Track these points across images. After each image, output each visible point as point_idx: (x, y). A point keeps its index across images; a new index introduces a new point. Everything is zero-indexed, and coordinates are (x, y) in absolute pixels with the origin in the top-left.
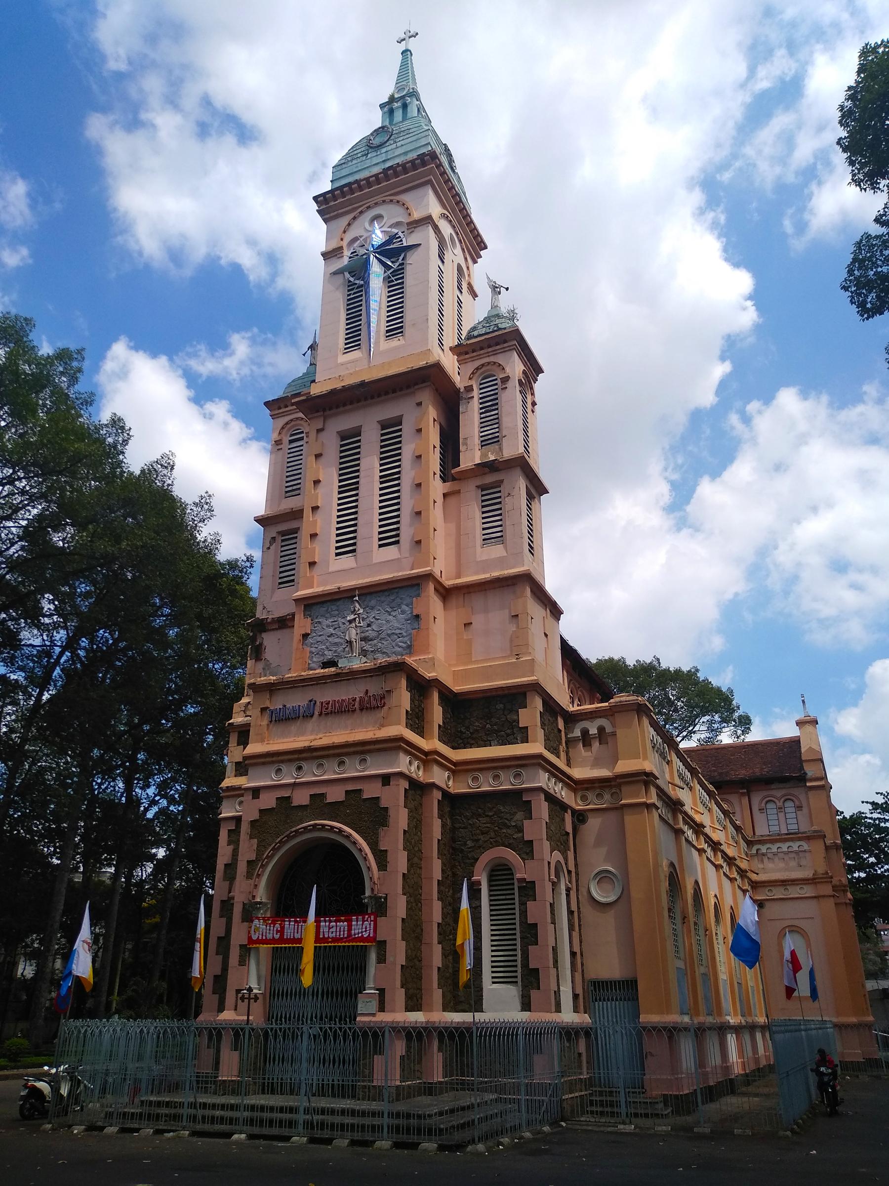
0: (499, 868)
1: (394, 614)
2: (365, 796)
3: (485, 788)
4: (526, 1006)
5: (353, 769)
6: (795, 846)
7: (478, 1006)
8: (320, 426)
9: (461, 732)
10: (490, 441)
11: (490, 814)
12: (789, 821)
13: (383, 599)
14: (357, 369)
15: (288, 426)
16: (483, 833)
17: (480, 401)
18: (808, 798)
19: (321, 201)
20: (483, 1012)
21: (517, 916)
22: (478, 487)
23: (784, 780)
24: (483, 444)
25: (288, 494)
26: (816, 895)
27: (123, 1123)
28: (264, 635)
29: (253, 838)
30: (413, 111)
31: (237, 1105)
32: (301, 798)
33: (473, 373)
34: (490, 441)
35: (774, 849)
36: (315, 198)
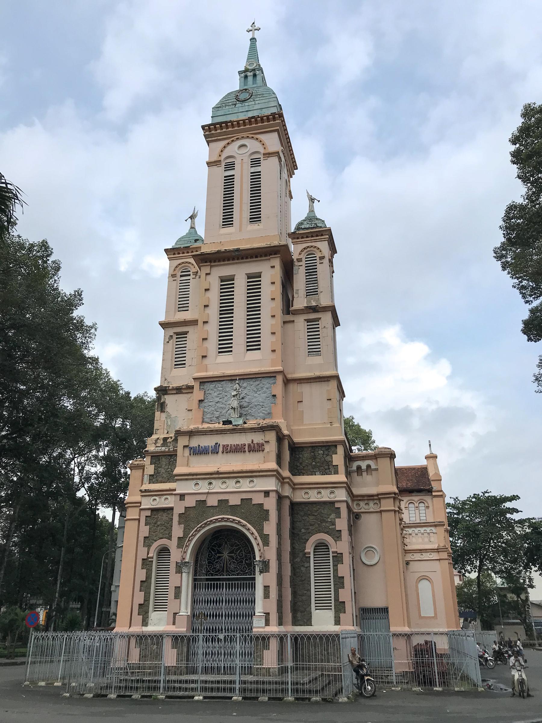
0: (320, 545)
1: (258, 393)
2: (253, 503)
3: (313, 499)
4: (337, 622)
5: (245, 485)
6: (428, 529)
7: (308, 623)
8: (208, 272)
9: (297, 466)
10: (312, 292)
11: (316, 514)
12: (421, 515)
13: (251, 383)
14: (231, 239)
15: (180, 266)
16: (311, 525)
17: (306, 268)
18: (433, 502)
19: (206, 129)
20: (311, 626)
21: (332, 572)
22: (305, 320)
23: (420, 491)
24: (308, 294)
25: (180, 309)
26: (438, 558)
27: (119, 692)
28: (166, 396)
29: (181, 524)
30: (259, 78)
31: (196, 680)
32: (212, 501)
33: (302, 251)
34: (312, 292)
35: (416, 531)
36: (203, 127)
